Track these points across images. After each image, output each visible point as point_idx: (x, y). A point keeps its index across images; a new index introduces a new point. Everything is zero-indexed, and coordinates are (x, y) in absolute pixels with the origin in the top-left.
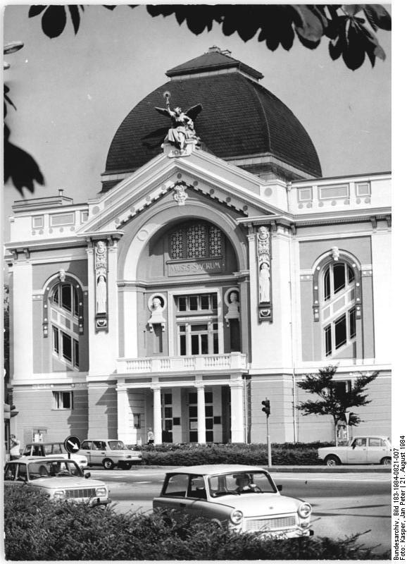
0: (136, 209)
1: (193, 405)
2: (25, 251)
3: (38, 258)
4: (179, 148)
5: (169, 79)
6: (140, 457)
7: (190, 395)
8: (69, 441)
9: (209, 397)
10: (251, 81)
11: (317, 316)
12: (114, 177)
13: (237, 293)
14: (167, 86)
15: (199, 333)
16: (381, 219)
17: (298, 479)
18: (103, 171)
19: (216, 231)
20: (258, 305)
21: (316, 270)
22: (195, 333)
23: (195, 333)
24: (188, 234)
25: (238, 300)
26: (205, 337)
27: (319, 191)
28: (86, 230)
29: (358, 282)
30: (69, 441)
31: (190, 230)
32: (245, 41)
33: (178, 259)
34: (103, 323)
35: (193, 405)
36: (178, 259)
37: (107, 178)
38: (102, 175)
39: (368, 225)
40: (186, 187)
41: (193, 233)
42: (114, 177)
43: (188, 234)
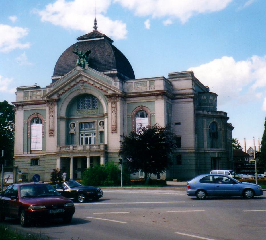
3: (26, 108)
5: (78, 41)
6: (134, 174)
7: (84, 159)
8: (35, 176)
9: (91, 161)
12: (57, 78)
13: (103, 122)
14: (77, 43)
17: (114, 191)
18: (53, 75)
19: (95, 99)
20: (112, 126)
25: (103, 124)
26: (90, 139)
27: (149, 83)
29: (133, 121)
30: (35, 176)
33: (89, 108)
36: (89, 108)
37: (54, 78)
38: (52, 76)
39: (154, 97)
41: (87, 100)
42: (57, 78)
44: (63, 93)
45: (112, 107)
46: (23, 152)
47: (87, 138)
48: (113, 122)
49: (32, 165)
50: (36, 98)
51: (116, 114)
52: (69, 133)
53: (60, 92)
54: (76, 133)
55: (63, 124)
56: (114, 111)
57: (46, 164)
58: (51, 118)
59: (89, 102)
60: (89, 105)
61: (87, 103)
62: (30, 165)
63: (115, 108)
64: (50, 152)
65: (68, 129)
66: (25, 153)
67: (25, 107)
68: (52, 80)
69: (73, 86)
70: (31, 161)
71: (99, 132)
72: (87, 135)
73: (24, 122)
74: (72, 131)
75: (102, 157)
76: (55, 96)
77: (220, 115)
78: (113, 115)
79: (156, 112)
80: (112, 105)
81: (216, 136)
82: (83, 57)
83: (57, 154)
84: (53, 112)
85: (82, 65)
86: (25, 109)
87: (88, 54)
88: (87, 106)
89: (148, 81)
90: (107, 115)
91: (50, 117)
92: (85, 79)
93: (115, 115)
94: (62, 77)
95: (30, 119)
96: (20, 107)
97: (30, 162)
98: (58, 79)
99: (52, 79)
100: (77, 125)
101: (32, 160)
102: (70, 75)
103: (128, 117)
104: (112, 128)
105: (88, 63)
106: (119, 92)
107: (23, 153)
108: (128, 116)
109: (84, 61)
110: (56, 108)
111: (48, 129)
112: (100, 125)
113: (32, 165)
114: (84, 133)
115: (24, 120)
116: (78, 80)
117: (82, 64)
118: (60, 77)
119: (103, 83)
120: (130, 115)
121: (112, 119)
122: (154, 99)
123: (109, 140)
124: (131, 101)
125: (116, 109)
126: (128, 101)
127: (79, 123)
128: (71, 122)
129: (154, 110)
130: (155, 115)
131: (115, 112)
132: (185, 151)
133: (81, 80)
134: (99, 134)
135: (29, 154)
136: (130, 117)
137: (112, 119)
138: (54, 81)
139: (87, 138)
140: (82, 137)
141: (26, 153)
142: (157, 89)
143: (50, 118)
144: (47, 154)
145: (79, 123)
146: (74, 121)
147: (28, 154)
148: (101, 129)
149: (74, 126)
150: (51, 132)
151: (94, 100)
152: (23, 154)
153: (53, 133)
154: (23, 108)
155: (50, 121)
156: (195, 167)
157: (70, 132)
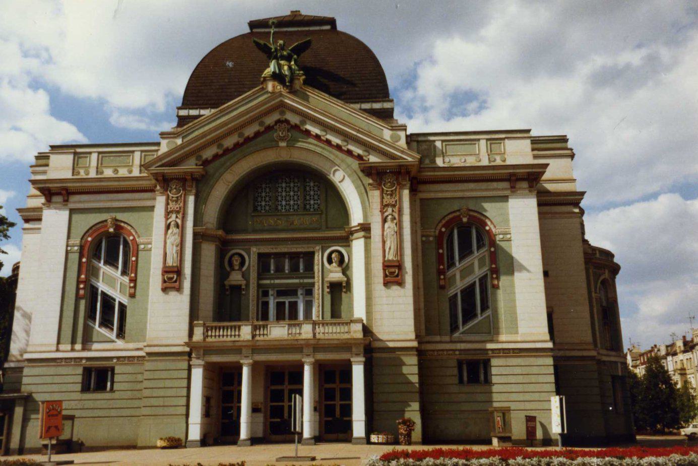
0: (246, 134)
1: (238, 405)
2: (64, 192)
4: (306, 70)
10: (251, 112)
11: (442, 283)
12: (193, 112)
15: (287, 300)
16: (39, 419)
18: (180, 105)
21: (440, 231)
22: (281, 300)
23: (281, 300)
24: (277, 185)
28: (157, 165)
31: (280, 181)
32: (3, 265)
34: (172, 278)
35: (238, 405)
37: (183, 113)
38: (179, 108)
39: (506, 185)
40: (289, 127)
41: (284, 185)
42: (193, 112)
43: (277, 185)
44: (216, 157)
45: (385, 203)
46: (58, 343)
47: (284, 303)
48: (387, 250)
49: (86, 388)
50: (116, 171)
51: (400, 225)
52: (224, 285)
53: (208, 154)
54: (247, 285)
55: (209, 251)
56: (390, 217)
57: (147, 384)
58: (173, 230)
59: (292, 193)
60: (292, 202)
61: (284, 194)
62: (79, 387)
63: (394, 206)
64: (165, 342)
65: (222, 273)
66: (62, 347)
67: (74, 198)
68: (177, 119)
69: (252, 135)
70: (83, 375)
71: (326, 285)
72: (280, 293)
73: (67, 246)
74: (236, 278)
75: (358, 363)
76: (190, 166)
77: (270, 294)
78: (389, 227)
79: (513, 231)
80: (382, 198)
81: (469, 317)
82: (288, 59)
83: (192, 351)
84: (178, 212)
85: (286, 75)
86: (75, 202)
87: (298, 50)
88: (284, 203)
89: (485, 141)
90: (365, 228)
91: (168, 227)
92: (294, 119)
93: (396, 229)
94: (213, 111)
95: (90, 236)
96: (57, 199)
97: (79, 379)
98: (200, 116)
99: (178, 116)
100: (252, 261)
101: (87, 371)
102: (240, 107)
103: (423, 242)
104: (384, 270)
105: (303, 75)
106: (410, 159)
107: (54, 348)
108: (424, 239)
109: (290, 67)
110: (191, 199)
111: (161, 266)
112: (330, 261)
113: (86, 388)
114: (273, 286)
115: (69, 237)
116: (270, 120)
117: (287, 73)
118: (206, 112)
119: (358, 131)
120: (431, 236)
121: (384, 242)
122: (506, 189)
123: (376, 308)
124: (430, 191)
125: (396, 209)
126: (424, 192)
127: (260, 255)
128: (230, 250)
129: (506, 221)
130: (508, 236)
131: (395, 219)
132: (568, 354)
133: (278, 122)
134: (326, 290)
135: (78, 351)
136: (430, 242)
137: (384, 242)
138: (182, 121)
139: (284, 303)
140: (265, 299)
141: (69, 347)
142: (512, 160)
143: (170, 231)
144: (149, 350)
145: (260, 255)
146: (243, 249)
147: (73, 350)
148: (335, 275)
149: (242, 263)
150: (171, 275)
151: (308, 189)
152: (58, 350)
153: (176, 282)
154: (66, 201)
155: (168, 241)
156: (492, 393)
157: (226, 283)
